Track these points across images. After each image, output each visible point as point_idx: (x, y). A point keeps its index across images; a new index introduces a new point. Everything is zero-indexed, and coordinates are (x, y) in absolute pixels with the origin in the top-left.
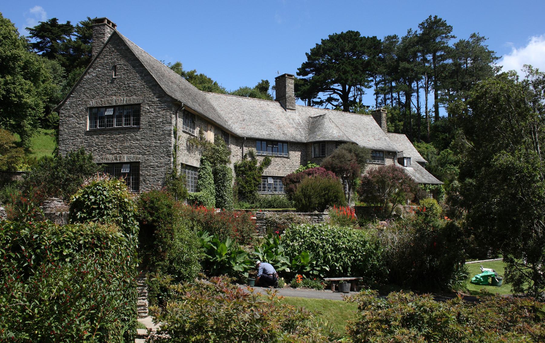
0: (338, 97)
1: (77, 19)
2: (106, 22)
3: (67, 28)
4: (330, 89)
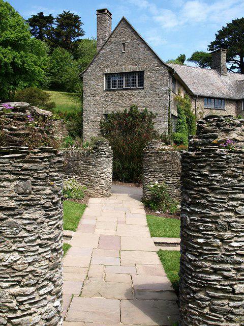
0: (237, 66)
1: (56, 13)
2: (106, 12)
3: (50, 19)
4: (234, 60)
